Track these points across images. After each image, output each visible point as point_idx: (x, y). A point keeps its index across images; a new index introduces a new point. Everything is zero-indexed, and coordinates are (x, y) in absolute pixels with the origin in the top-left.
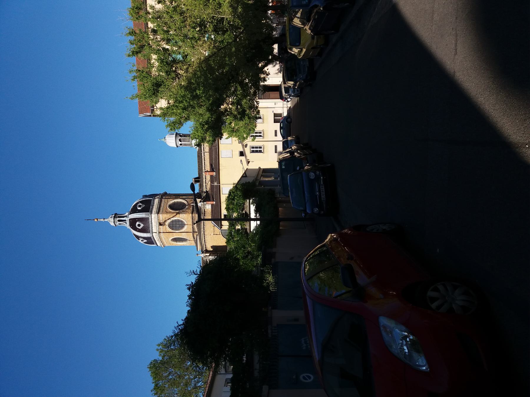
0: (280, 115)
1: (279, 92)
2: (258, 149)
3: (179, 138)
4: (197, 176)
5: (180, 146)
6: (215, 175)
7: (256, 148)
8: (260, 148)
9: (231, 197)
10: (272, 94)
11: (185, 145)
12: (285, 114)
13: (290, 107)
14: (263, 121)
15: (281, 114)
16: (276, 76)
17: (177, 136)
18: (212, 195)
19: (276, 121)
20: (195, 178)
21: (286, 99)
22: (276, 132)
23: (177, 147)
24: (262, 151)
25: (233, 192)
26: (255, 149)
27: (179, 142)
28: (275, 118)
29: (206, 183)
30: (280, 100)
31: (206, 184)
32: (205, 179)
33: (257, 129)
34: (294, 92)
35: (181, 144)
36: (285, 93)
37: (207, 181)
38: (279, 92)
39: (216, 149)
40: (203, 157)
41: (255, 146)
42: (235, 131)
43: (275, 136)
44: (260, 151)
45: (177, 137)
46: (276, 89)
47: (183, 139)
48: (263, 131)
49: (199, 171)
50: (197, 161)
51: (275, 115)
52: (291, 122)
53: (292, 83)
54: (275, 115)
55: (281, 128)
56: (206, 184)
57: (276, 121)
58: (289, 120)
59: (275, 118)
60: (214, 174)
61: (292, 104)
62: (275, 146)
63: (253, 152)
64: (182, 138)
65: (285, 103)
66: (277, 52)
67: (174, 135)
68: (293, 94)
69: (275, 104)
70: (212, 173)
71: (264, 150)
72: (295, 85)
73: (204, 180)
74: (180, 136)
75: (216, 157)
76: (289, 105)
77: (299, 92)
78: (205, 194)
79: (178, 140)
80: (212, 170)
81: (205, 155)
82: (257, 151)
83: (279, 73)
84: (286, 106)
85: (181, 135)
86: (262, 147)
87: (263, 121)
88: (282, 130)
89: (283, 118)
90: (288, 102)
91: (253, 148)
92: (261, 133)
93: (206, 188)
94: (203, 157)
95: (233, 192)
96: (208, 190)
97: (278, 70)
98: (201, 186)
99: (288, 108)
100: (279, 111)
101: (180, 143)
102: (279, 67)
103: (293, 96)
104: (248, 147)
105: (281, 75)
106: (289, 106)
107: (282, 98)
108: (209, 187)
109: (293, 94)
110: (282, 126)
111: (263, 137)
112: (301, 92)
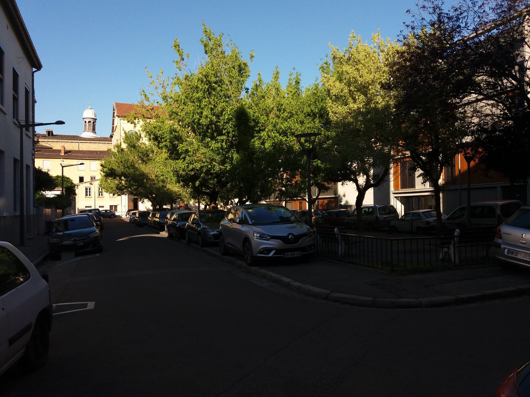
0: (116, 210)
1: (133, 209)
2: (88, 193)
3: (92, 122)
4: (54, 134)
5: (84, 121)
6: (61, 155)
7: (90, 192)
8: (90, 195)
9: (66, 179)
10: (132, 204)
11: (85, 126)
12: (117, 214)
13: (122, 217)
14: (111, 197)
15: (116, 210)
16: (145, 207)
17: (94, 120)
18: (40, 150)
19: (111, 207)
20: (52, 132)
21: (128, 214)
22: (103, 207)
23: (83, 119)
24: (86, 196)
25: (69, 181)
26: (88, 190)
27: (88, 121)
28: (114, 206)
29: (47, 141)
30: (127, 210)
31: (46, 142)
32: (52, 142)
33: (105, 194)
34: (133, 218)
35: (86, 122)
36: (132, 213)
37: (50, 142)
38: (133, 209)
39: (85, 157)
40: (74, 141)
41: (91, 190)
42: (106, 180)
43: (86, 206)
44: (87, 195)
45: (93, 120)
46: (136, 207)
47: (91, 124)
48: (103, 197)
49: (59, 135)
50: (70, 135)
51: (116, 206)
52: (110, 218)
53: (138, 216)
54: (116, 206)
55: (106, 211)
56: (46, 142)
57: (111, 207)
58: (113, 216)
59: (114, 206)
60: (63, 154)
61: (125, 218)
62: (104, 206)
63: (86, 189)
64: (92, 124)
65: (125, 213)
66: (204, 208)
67: (94, 117)
68: (131, 217)
69: (124, 206)
70: (63, 152)
71: (87, 197)
72: (137, 217)
73: (51, 141)
74: (94, 123)
75: (78, 156)
76: (124, 217)
77: (133, 221)
78: (36, 140)
79: (90, 120)
80: (66, 152)
81: (76, 143)
82: (87, 192)
83: (146, 209)
84: (123, 214)
85: (95, 123)
86: (90, 196)
87: (111, 197)
88: (104, 211)
89: (114, 212)
90: (126, 215)
91: (90, 189)
92: (102, 195)
93: (42, 141)
94: (74, 141)
95: (69, 181)
96: (40, 143)
97: (149, 208)
98: (44, 136)
99: (121, 216)
100: (119, 208)
101: (87, 122)
102: (151, 209)
103: (130, 217)
104: (91, 186)
105: (145, 210)
106: (123, 216)
107: (129, 211)
108: (44, 144)
109: (131, 217)
110: (108, 211)
111: (99, 197)
112: (133, 223)
